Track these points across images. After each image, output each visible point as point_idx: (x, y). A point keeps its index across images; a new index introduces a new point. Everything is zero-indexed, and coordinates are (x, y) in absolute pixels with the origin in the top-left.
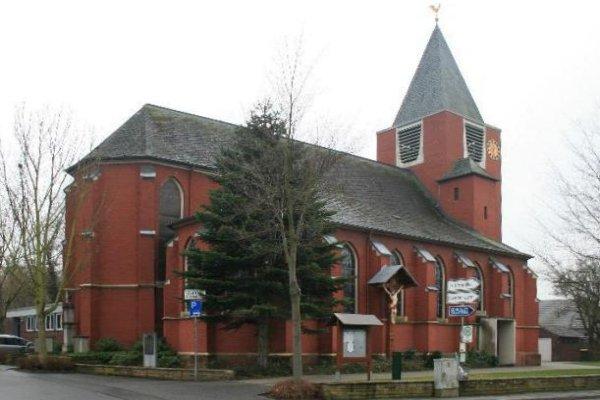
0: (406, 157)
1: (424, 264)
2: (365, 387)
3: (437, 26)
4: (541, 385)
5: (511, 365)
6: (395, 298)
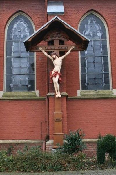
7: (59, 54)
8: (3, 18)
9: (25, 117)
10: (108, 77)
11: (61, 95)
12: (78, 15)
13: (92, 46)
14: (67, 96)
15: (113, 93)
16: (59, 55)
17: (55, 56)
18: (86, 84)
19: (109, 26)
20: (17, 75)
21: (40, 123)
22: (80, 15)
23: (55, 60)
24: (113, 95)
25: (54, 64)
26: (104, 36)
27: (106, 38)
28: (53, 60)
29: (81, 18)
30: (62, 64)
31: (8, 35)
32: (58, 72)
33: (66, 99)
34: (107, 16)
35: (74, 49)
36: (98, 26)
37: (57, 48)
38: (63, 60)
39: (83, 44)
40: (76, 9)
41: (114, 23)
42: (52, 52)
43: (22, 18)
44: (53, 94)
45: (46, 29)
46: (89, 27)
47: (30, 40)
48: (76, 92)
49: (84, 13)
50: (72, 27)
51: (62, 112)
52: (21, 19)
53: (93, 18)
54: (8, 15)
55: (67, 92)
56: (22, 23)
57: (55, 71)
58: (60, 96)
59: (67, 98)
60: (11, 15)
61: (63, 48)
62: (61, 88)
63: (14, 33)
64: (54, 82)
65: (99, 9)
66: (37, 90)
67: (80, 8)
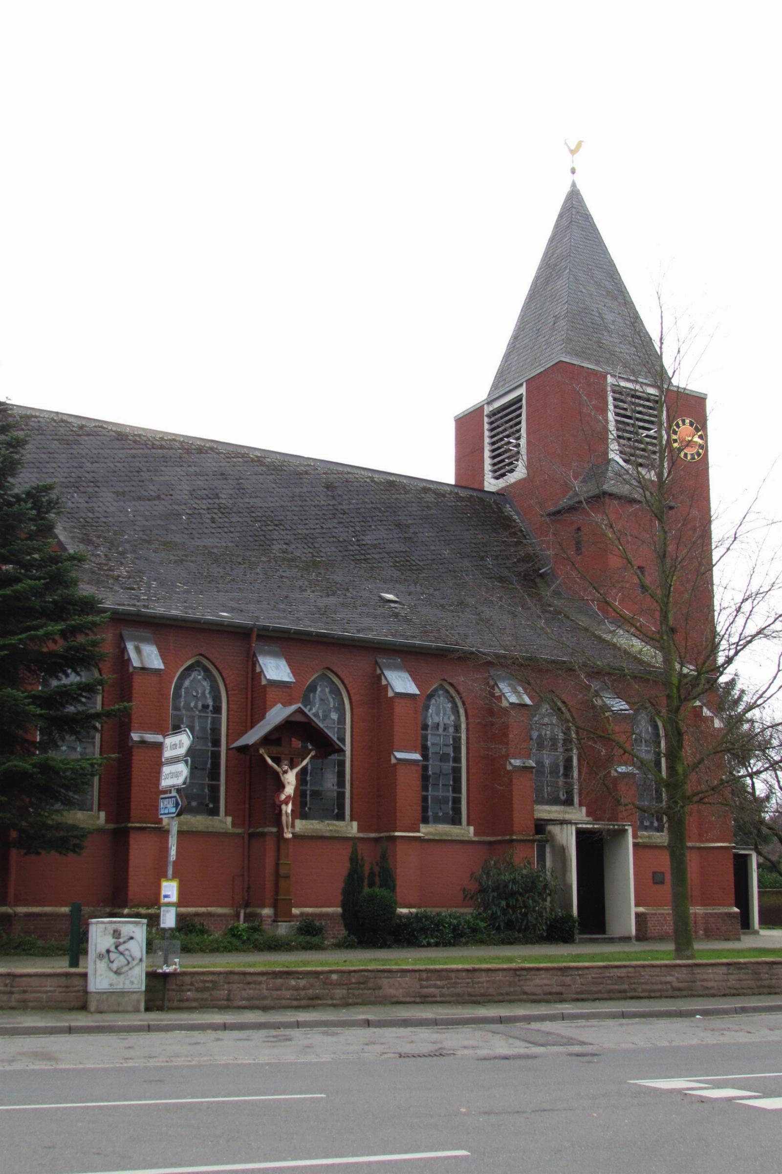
0: (501, 470)
1: (505, 710)
2: (511, 972)
3: (574, 185)
4: (732, 981)
5: (626, 939)
6: (290, 779)
10: (344, 798)
19: (354, 704)
23: (285, 775)
26: (342, 720)
27: (344, 724)
28: (283, 774)
36: (333, 698)
46: (317, 700)
57: (287, 794)
66: (226, 814)
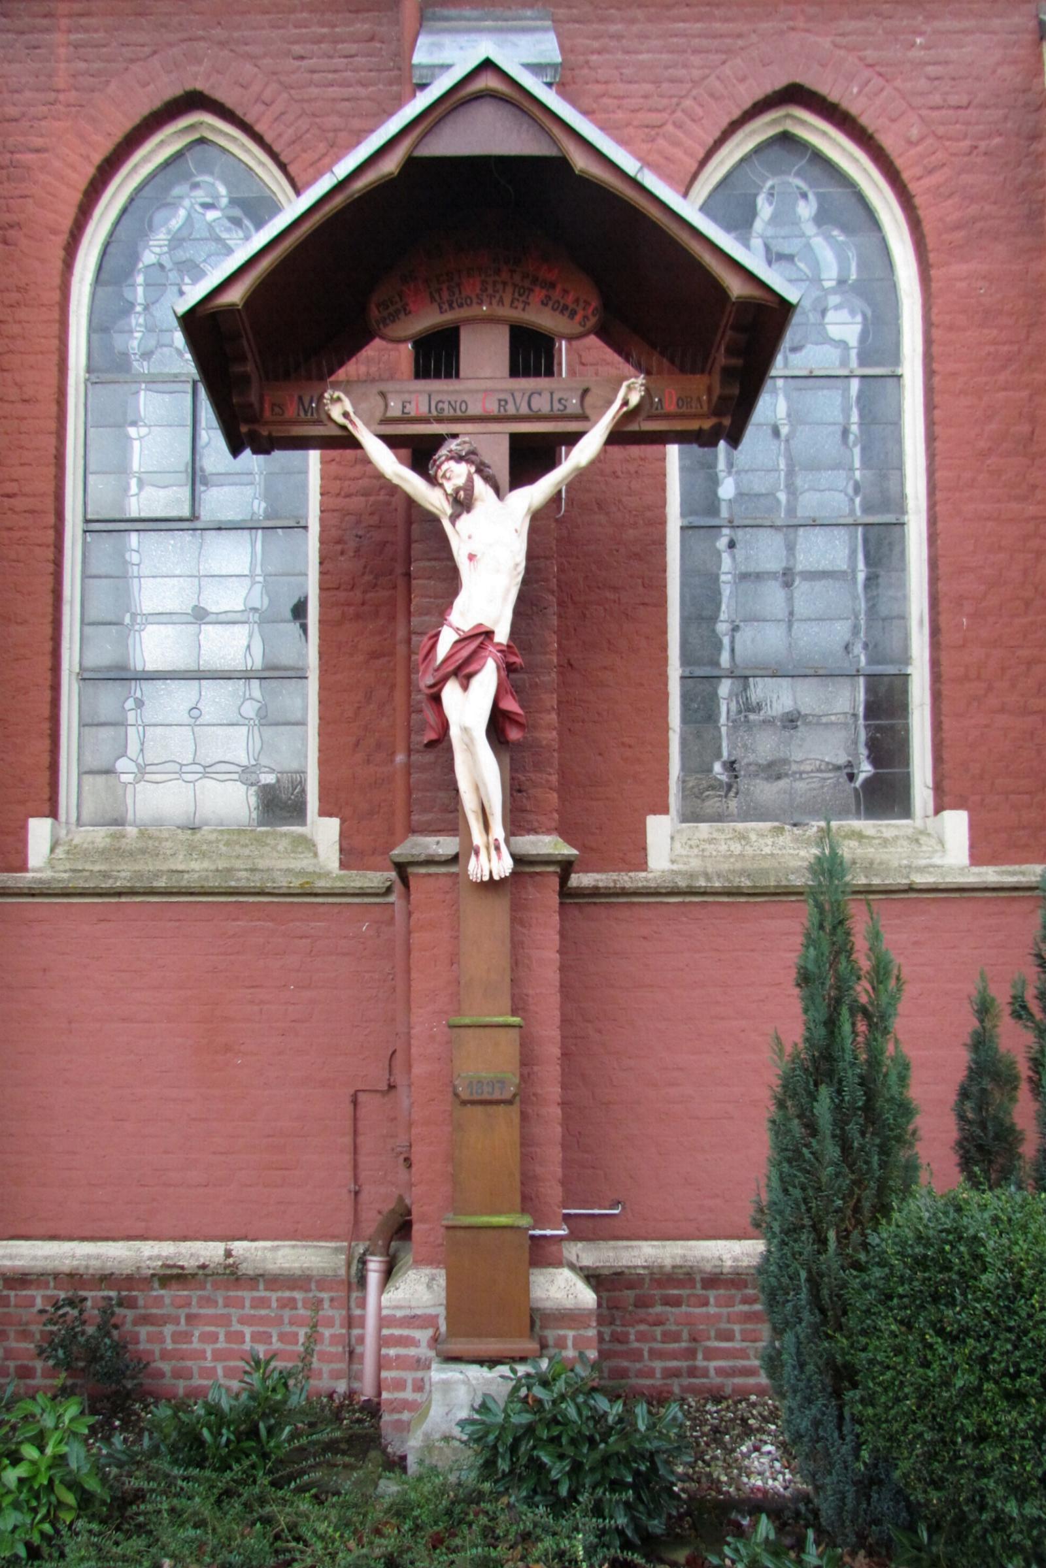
7: (499, 459)
8: (57, 164)
9: (227, 1048)
11: (513, 856)
12: (676, 143)
13: (776, 432)
14: (566, 867)
15: (941, 842)
16: (504, 477)
17: (470, 480)
18: (717, 767)
19: (931, 241)
20: (173, 685)
21: (348, 1099)
22: (688, 142)
23: (465, 520)
24: (937, 860)
25: (460, 550)
28: (454, 518)
29: (703, 163)
30: (530, 556)
31: (99, 327)
32: (489, 634)
33: (556, 899)
34: (913, 152)
35: (638, 407)
37: (493, 408)
38: (539, 521)
39: (721, 359)
40: (657, 82)
41: (974, 209)
42: (437, 441)
43: (211, 173)
44: (445, 846)
45: (387, 186)
47: (235, 296)
48: (642, 831)
49: (724, 122)
50: (628, 163)
51: (516, 1020)
52: (207, 178)
53: (798, 174)
54: (98, 138)
55: (565, 832)
56: (211, 215)
57: (467, 626)
58: (503, 866)
59: (566, 892)
60: (118, 135)
61: (542, 404)
62: (514, 790)
63: (146, 308)
64: (454, 732)
65: (851, 78)
66: (323, 813)
67: (696, 74)
